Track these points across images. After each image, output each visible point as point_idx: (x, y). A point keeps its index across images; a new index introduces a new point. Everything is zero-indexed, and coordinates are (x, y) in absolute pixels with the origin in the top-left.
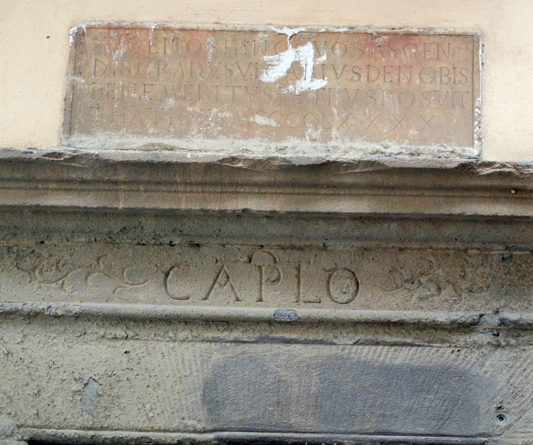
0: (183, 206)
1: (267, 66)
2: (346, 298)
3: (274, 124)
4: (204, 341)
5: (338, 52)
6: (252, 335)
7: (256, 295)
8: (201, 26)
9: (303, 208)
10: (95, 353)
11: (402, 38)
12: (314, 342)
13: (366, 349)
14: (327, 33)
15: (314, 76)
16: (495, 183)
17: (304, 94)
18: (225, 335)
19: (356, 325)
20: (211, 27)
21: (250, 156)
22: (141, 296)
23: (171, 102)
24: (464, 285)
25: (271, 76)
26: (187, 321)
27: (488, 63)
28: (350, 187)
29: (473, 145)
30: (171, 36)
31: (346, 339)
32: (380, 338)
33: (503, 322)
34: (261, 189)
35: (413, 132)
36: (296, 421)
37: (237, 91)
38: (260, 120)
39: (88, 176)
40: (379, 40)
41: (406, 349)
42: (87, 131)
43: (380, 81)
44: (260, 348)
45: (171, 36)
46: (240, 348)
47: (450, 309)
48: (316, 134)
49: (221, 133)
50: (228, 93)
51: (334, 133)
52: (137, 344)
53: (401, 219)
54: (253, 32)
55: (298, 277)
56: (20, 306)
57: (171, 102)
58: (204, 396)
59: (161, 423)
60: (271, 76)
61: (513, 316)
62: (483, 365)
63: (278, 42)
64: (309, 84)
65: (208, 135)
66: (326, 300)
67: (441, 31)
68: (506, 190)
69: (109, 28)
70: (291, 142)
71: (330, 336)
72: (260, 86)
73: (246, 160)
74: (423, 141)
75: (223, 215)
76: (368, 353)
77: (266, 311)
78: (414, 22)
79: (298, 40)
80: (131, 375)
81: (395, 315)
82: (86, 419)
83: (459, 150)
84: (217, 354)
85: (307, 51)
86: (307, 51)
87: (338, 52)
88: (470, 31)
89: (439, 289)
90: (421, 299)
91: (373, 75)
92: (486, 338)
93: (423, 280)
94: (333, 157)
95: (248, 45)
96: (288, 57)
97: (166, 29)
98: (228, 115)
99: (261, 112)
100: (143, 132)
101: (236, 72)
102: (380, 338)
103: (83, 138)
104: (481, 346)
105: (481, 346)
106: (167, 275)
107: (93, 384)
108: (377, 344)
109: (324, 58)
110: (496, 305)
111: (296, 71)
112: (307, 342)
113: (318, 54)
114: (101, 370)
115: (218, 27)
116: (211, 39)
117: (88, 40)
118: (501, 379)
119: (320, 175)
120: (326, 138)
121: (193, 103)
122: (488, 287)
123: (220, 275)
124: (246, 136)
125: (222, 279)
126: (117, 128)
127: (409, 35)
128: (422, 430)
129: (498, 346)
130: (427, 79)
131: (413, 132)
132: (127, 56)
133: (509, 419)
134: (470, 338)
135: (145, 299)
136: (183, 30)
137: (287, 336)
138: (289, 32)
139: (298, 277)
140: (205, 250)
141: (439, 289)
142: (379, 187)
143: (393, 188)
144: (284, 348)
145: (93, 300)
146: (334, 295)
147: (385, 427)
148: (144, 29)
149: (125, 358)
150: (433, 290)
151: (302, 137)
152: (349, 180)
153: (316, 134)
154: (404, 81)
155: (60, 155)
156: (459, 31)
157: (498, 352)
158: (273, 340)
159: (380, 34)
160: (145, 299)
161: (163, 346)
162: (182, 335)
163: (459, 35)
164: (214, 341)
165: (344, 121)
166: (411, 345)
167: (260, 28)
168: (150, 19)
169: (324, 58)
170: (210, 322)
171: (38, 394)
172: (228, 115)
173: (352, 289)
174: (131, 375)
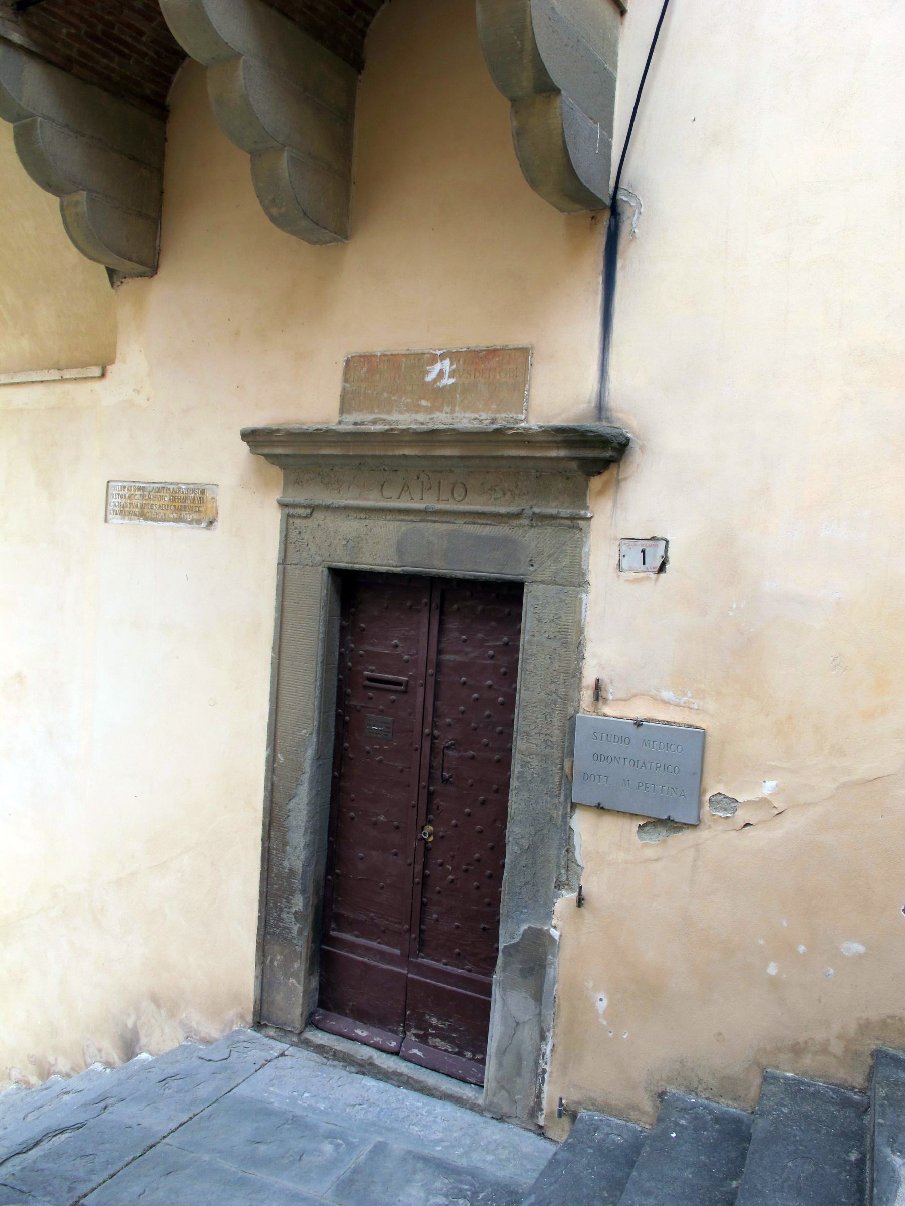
0: (377, 453)
1: (428, 372)
2: (460, 499)
3: (429, 404)
4: (398, 520)
5: (461, 362)
6: (418, 518)
7: (420, 497)
8: (400, 352)
9: (429, 454)
10: (351, 526)
11: (492, 352)
12: (446, 522)
13: (470, 526)
14: (457, 352)
15: (449, 377)
16: (516, 438)
17: (444, 387)
18: (406, 518)
19: (464, 514)
20: (404, 352)
21: (400, 427)
22: (371, 497)
23: (385, 395)
24: (517, 492)
25: (430, 378)
26: (391, 510)
27: (535, 364)
28: (448, 441)
29: (522, 413)
30: (386, 359)
31: (460, 521)
32: (476, 520)
33: (534, 513)
34: (410, 443)
35: (494, 406)
36: (436, 563)
37: (415, 388)
38: (424, 403)
39: (335, 439)
40: (481, 354)
41: (488, 527)
42: (349, 412)
43: (480, 378)
44: (422, 525)
45: (386, 359)
46: (414, 524)
47: (509, 505)
48: (448, 410)
49: (406, 410)
50: (409, 388)
51: (457, 408)
52: (370, 521)
53: (480, 457)
54: (423, 354)
55: (439, 487)
56: (321, 502)
57: (385, 395)
58: (397, 549)
59: (378, 561)
60: (430, 378)
61: (537, 510)
62: (524, 537)
63: (434, 359)
64: (448, 381)
65: (401, 412)
66: (451, 500)
67: (511, 347)
68: (524, 441)
69: (361, 356)
70: (437, 414)
71: (453, 519)
72: (425, 384)
73: (398, 429)
74: (498, 411)
75: (394, 456)
76: (470, 528)
77: (421, 505)
78: (498, 342)
79: (443, 357)
80: (367, 537)
81: (486, 509)
82: (348, 559)
83: (515, 416)
84: (404, 527)
85: (447, 362)
86: (447, 362)
87: (461, 362)
88: (525, 346)
89: (504, 494)
90: (495, 499)
91: (477, 374)
92: (526, 521)
93: (497, 489)
94: (436, 427)
95: (421, 360)
96: (438, 367)
97: (385, 355)
98: (409, 401)
99: (424, 398)
100: (372, 412)
101: (414, 376)
102: (476, 520)
103: (348, 416)
104: (524, 526)
105: (524, 526)
106: (382, 486)
107: (351, 542)
108: (475, 523)
109: (454, 366)
110: (531, 503)
111: (441, 374)
112: (443, 522)
113: (451, 365)
114: (354, 534)
115: (407, 352)
116: (404, 359)
117: (352, 364)
118: (533, 544)
119: (432, 436)
120: (453, 411)
121: (394, 395)
122: (529, 493)
123: (406, 488)
124: (417, 412)
125: (406, 489)
126: (361, 411)
127: (495, 350)
128: (493, 571)
129: (532, 526)
130: (503, 375)
131: (494, 406)
132: (368, 371)
133: (536, 566)
134: (516, 522)
135: (372, 500)
136: (392, 355)
137: (434, 519)
138: (439, 353)
139: (439, 487)
140: (399, 473)
141: (504, 494)
142: (462, 441)
143: (469, 442)
144: (433, 524)
145: (352, 499)
146: (455, 496)
147: (476, 568)
148: (376, 356)
149: (365, 529)
150: (501, 493)
151: (442, 411)
152: (447, 438)
153: (448, 410)
154: (492, 377)
155: (321, 429)
156: (520, 346)
157: (533, 530)
158: (428, 521)
159: (481, 351)
160: (372, 500)
161: (381, 523)
162: (388, 517)
163: (520, 349)
164: (401, 520)
165: (462, 401)
166: (490, 524)
167: (426, 352)
168: (378, 350)
169: (454, 366)
170: (401, 511)
171: (330, 546)
172: (409, 401)
173: (463, 494)
174: (367, 537)
